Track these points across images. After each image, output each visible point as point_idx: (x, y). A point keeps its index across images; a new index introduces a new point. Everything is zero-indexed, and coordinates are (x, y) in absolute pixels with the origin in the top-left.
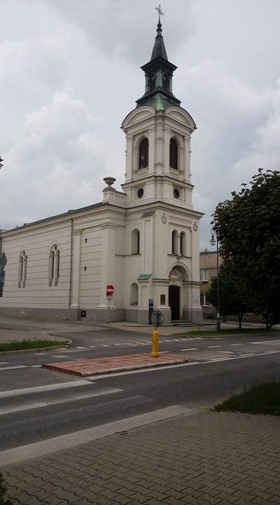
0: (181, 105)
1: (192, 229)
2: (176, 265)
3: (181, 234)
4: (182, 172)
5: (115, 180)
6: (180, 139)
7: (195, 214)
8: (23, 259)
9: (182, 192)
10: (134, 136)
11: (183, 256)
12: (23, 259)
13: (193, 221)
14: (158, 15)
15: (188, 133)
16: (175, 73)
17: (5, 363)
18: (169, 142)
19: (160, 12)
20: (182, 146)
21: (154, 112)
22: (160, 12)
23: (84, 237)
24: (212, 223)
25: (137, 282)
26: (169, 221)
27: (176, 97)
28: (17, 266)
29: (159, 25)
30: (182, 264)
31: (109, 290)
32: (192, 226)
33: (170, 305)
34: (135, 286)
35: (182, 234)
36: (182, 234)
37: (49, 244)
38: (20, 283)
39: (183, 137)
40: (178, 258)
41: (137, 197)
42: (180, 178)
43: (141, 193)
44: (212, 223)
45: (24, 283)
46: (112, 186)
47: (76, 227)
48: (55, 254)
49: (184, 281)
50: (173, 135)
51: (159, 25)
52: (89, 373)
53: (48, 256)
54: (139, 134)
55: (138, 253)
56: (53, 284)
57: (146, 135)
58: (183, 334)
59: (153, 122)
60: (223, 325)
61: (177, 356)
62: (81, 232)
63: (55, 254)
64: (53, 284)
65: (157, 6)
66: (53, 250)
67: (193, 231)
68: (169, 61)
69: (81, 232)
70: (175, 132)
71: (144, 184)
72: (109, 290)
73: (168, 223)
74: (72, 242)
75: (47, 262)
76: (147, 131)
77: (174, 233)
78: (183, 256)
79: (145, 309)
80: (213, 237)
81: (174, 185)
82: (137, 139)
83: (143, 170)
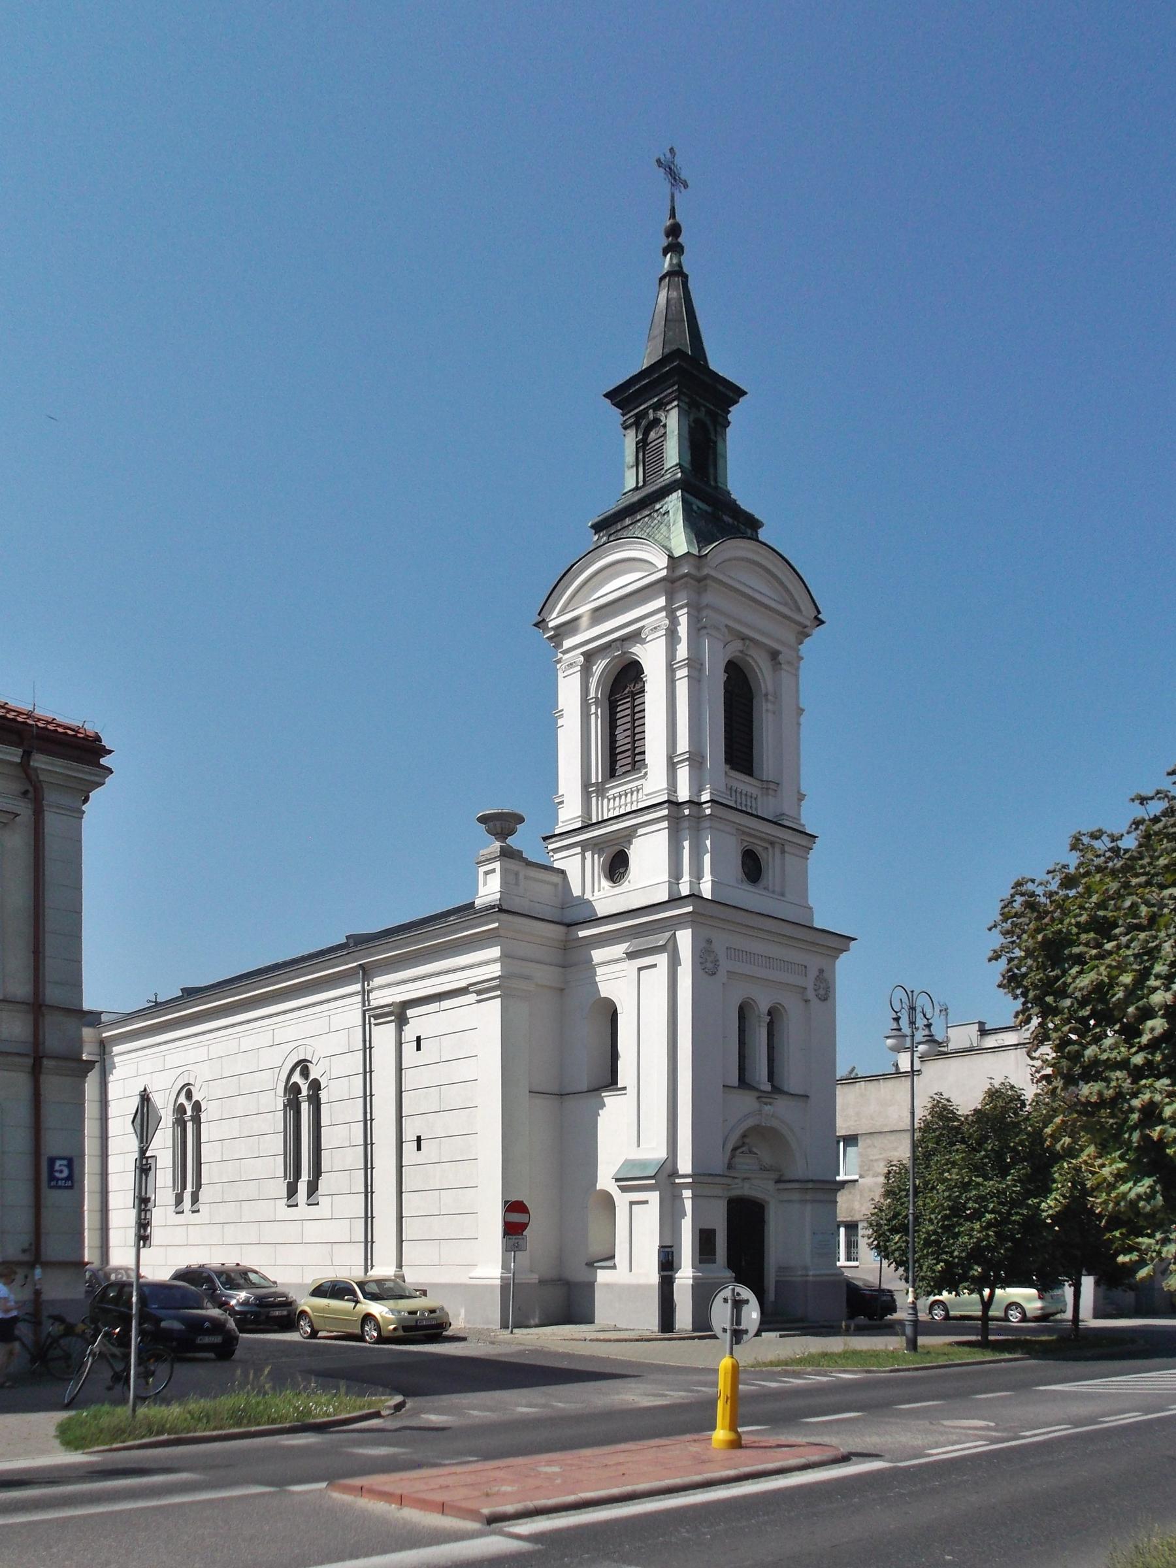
0: (762, 534)
1: (810, 994)
2: (750, 1122)
3: (769, 1013)
4: (771, 787)
5: (521, 820)
6: (761, 665)
9: (772, 863)
11: (777, 1090)
13: (814, 962)
14: (665, 187)
15: (791, 638)
16: (735, 414)
17: (184, 1476)
18: (722, 677)
19: (674, 177)
20: (770, 688)
22: (674, 177)
24: (996, 957)
26: (725, 965)
27: (744, 506)
29: (674, 231)
30: (775, 1123)
31: (516, 1217)
32: (809, 983)
35: (774, 1014)
36: (774, 1014)
37: (280, 1060)
39: (774, 655)
40: (762, 1096)
42: (766, 807)
43: (617, 867)
44: (996, 957)
46: (510, 841)
47: (380, 998)
48: (302, 1097)
49: (778, 1181)
50: (737, 645)
51: (674, 231)
52: (510, 1508)
54: (608, 645)
58: (800, 1361)
61: (783, 1439)
62: (399, 1014)
63: (302, 1097)
65: (663, 153)
66: (182, 1099)
67: (815, 1001)
68: (713, 366)
69: (399, 1014)
70: (744, 638)
71: (629, 834)
72: (516, 1217)
73: (722, 972)
74: (367, 1048)
77: (743, 1012)
78: (777, 1090)
79: (642, 1281)
80: (897, 1019)
81: (742, 832)
82: (599, 667)
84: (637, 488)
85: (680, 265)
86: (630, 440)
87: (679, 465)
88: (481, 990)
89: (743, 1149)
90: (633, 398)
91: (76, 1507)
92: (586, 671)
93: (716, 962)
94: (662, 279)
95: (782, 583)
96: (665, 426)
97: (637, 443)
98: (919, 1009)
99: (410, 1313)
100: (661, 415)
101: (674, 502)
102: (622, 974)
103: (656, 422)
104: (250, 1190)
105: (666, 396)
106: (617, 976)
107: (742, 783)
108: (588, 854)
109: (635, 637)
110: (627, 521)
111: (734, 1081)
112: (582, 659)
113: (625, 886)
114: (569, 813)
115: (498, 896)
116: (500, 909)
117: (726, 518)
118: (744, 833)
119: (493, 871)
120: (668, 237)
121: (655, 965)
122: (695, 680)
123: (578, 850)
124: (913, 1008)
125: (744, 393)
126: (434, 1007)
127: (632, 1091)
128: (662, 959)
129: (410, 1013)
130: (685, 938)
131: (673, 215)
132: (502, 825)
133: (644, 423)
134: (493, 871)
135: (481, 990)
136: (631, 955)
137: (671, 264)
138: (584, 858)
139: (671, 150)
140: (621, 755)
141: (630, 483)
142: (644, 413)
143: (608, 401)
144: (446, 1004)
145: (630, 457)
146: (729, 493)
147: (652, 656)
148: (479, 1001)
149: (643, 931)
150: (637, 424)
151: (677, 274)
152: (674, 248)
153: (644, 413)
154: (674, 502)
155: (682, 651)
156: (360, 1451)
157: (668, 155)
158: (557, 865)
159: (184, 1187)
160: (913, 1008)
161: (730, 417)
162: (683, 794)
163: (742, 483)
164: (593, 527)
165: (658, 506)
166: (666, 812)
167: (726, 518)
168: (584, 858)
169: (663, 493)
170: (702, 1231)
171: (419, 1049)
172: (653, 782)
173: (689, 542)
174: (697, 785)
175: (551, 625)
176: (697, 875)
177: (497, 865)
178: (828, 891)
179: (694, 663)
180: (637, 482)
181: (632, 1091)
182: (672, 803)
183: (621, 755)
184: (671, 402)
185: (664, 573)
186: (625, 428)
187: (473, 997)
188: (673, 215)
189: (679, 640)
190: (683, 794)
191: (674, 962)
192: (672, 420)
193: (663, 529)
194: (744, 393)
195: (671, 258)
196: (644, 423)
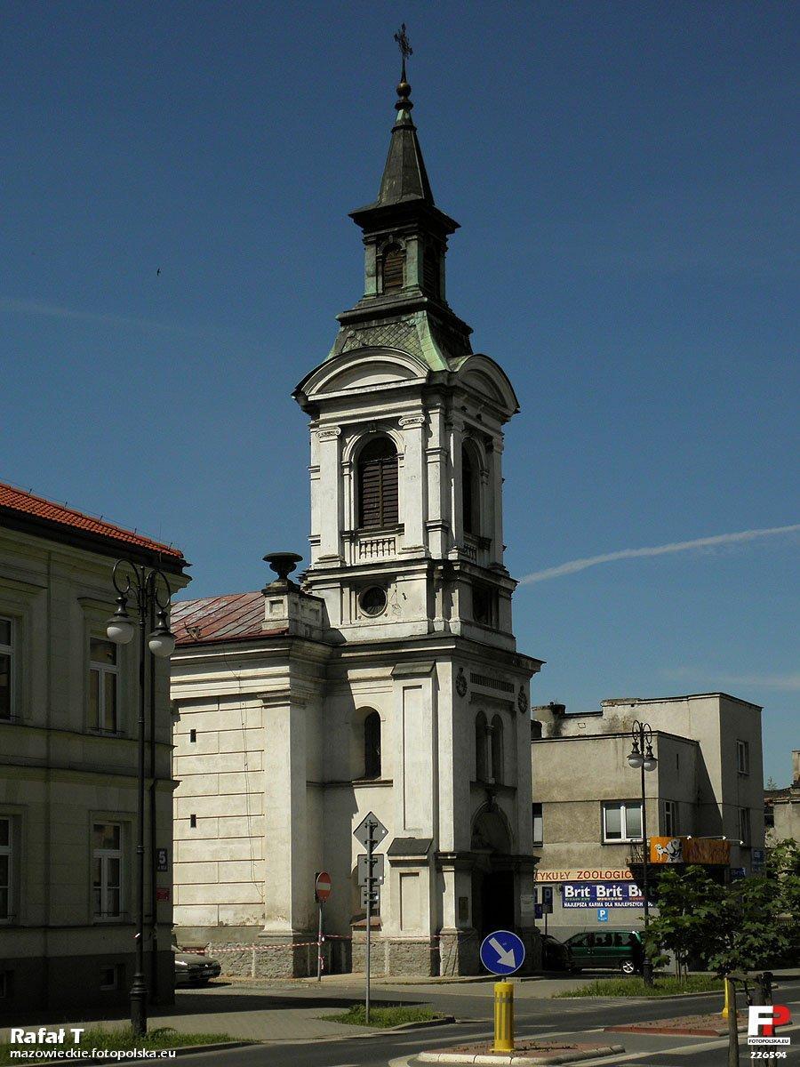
16: (452, 240)
19: (406, 50)
22: (406, 50)
65: (397, 29)
68: (437, 206)
82: (351, 441)
85: (410, 120)
86: (370, 256)
88: (270, 699)
92: (341, 439)
93: (465, 685)
94: (395, 130)
95: (493, 383)
96: (405, 251)
99: (200, 965)
102: (390, 689)
104: (232, 827)
105: (406, 229)
106: (371, 690)
108: (347, 590)
109: (393, 423)
110: (374, 323)
117: (451, 329)
121: (420, 687)
122: (445, 462)
126: (237, 705)
128: (427, 683)
129: (181, 710)
130: (445, 670)
131: (404, 78)
132: (283, 563)
133: (384, 244)
134: (281, 602)
135: (270, 699)
136: (396, 677)
137: (404, 119)
138: (342, 592)
139: (403, 26)
142: (385, 237)
143: (358, 230)
144: (223, 706)
148: (266, 707)
149: (399, 657)
150: (377, 243)
151: (408, 126)
152: (406, 105)
155: (434, 442)
158: (315, 594)
162: (436, 553)
163: (458, 301)
164: (339, 320)
165: (404, 318)
166: (426, 566)
167: (451, 329)
168: (342, 592)
170: (460, 899)
174: (446, 548)
176: (447, 615)
177: (285, 598)
178: (527, 628)
179: (444, 451)
182: (428, 559)
184: (411, 235)
185: (423, 381)
187: (259, 703)
188: (404, 78)
189: (431, 434)
191: (436, 687)
194: (459, 226)
195: (404, 114)
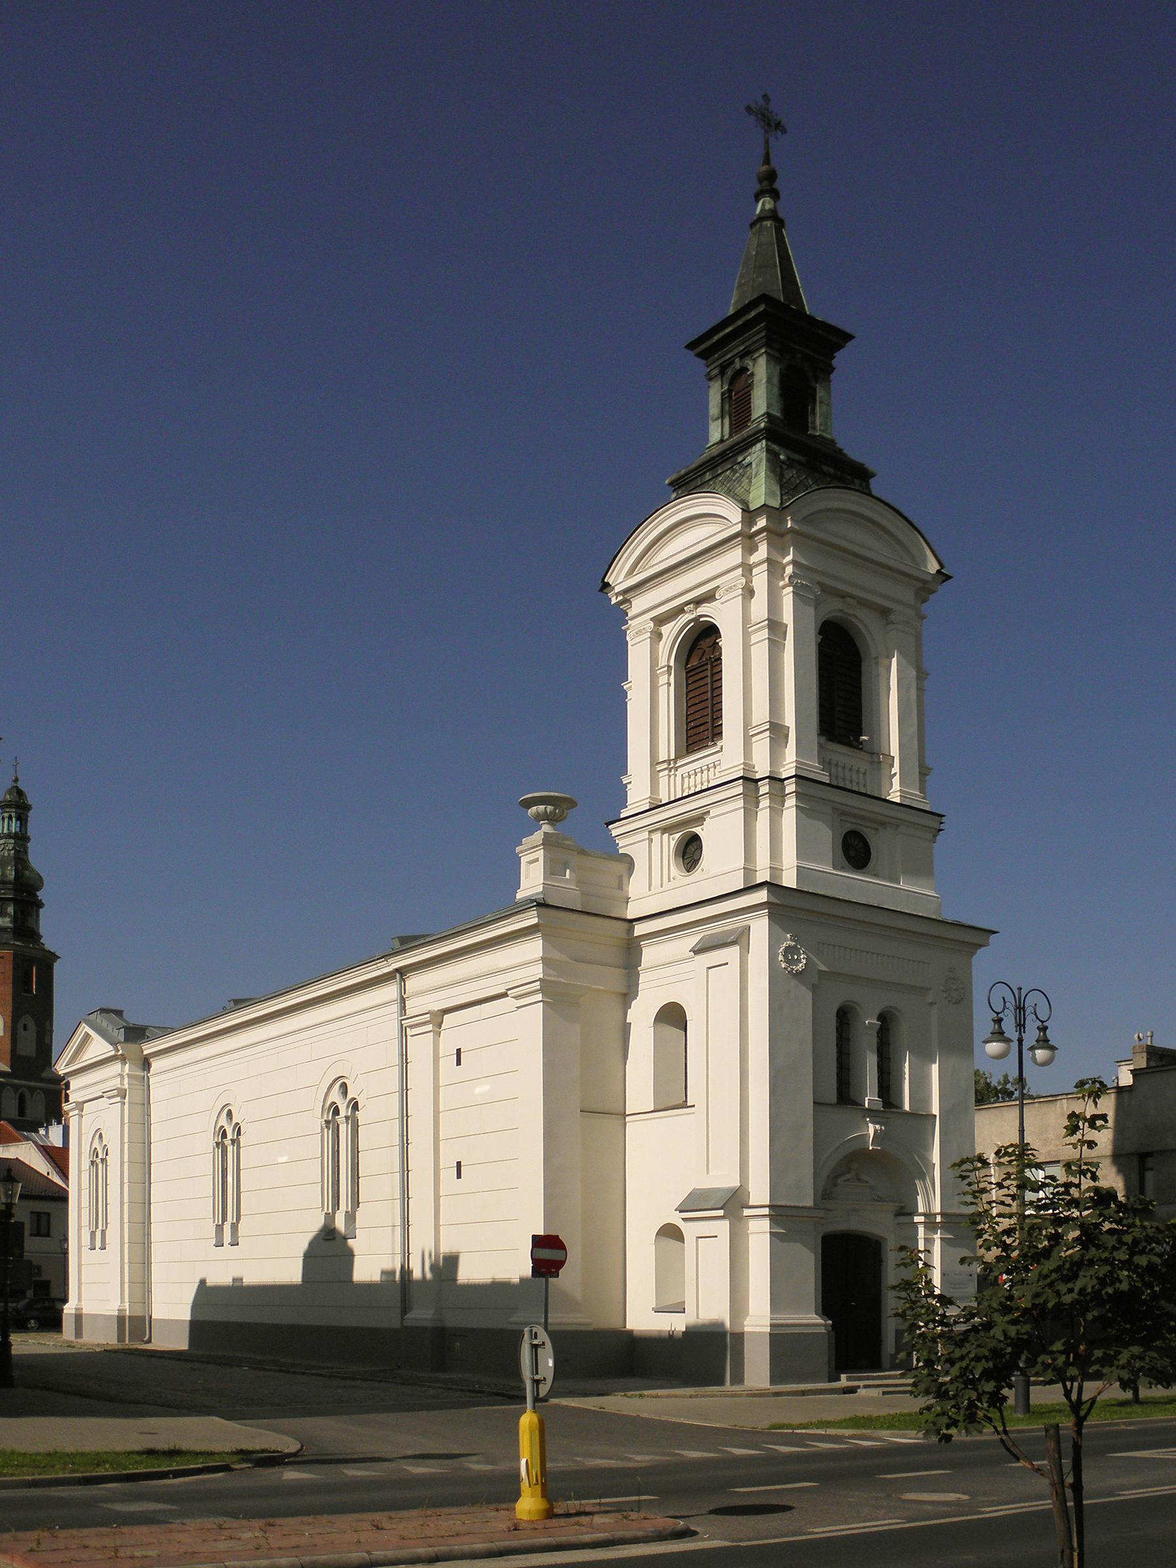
7: (860, 915)
8: (227, 1140)
10: (660, 621)
12: (227, 1140)
15: (908, 596)
21: (734, 514)
23: (449, 1041)
25: (676, 1219)
28: (205, 1163)
31: (546, 1254)
33: (826, 1309)
34: (670, 1232)
38: (219, 1229)
41: (674, 871)
43: (690, 851)
45: (235, 1227)
48: (340, 1117)
53: (316, 1121)
55: (684, 1105)
56: (227, 1237)
57: (711, 612)
59: (734, 556)
60: (1144, 1393)
63: (340, 1117)
64: (227, 1237)
72: (546, 1254)
75: (313, 1145)
76: (709, 597)
80: (999, 1021)
81: (842, 813)
82: (670, 631)
83: (702, 759)
84: (722, 441)
87: (768, 414)
89: (848, 1176)
90: (717, 347)
91: (686, 1552)
92: (657, 636)
97: (723, 394)
98: (1029, 1010)
100: (748, 362)
101: (757, 455)
103: (744, 369)
107: (839, 752)
111: (832, 1097)
112: (652, 624)
113: (697, 873)
114: (638, 793)
115: (540, 889)
116: (541, 904)
118: (843, 813)
119: (537, 860)
120: (761, 182)
123: (646, 835)
124: (1020, 1008)
125: (851, 337)
127: (700, 1108)
128: (731, 954)
131: (767, 160)
133: (730, 373)
134: (537, 860)
139: (765, 96)
140: (700, 724)
141: (715, 434)
145: (714, 407)
146: (833, 442)
147: (725, 615)
153: (731, 362)
154: (757, 455)
156: (952, 1497)
157: (761, 102)
159: (224, 1219)
160: (1020, 1008)
161: (834, 362)
164: (671, 484)
165: (740, 459)
168: (651, 840)
169: (745, 445)
171: (459, 1063)
172: (728, 756)
173: (770, 493)
175: (617, 589)
180: (722, 436)
181: (700, 1108)
183: (700, 724)
185: (738, 528)
186: (710, 379)
188: (767, 160)
190: (762, 768)
192: (761, 370)
193: (745, 481)
194: (851, 337)
196: (730, 373)
